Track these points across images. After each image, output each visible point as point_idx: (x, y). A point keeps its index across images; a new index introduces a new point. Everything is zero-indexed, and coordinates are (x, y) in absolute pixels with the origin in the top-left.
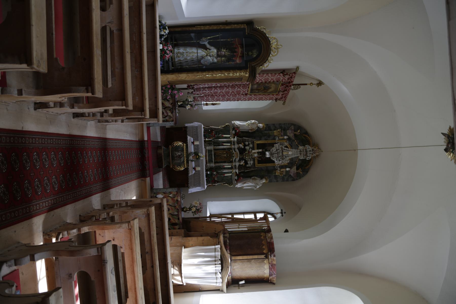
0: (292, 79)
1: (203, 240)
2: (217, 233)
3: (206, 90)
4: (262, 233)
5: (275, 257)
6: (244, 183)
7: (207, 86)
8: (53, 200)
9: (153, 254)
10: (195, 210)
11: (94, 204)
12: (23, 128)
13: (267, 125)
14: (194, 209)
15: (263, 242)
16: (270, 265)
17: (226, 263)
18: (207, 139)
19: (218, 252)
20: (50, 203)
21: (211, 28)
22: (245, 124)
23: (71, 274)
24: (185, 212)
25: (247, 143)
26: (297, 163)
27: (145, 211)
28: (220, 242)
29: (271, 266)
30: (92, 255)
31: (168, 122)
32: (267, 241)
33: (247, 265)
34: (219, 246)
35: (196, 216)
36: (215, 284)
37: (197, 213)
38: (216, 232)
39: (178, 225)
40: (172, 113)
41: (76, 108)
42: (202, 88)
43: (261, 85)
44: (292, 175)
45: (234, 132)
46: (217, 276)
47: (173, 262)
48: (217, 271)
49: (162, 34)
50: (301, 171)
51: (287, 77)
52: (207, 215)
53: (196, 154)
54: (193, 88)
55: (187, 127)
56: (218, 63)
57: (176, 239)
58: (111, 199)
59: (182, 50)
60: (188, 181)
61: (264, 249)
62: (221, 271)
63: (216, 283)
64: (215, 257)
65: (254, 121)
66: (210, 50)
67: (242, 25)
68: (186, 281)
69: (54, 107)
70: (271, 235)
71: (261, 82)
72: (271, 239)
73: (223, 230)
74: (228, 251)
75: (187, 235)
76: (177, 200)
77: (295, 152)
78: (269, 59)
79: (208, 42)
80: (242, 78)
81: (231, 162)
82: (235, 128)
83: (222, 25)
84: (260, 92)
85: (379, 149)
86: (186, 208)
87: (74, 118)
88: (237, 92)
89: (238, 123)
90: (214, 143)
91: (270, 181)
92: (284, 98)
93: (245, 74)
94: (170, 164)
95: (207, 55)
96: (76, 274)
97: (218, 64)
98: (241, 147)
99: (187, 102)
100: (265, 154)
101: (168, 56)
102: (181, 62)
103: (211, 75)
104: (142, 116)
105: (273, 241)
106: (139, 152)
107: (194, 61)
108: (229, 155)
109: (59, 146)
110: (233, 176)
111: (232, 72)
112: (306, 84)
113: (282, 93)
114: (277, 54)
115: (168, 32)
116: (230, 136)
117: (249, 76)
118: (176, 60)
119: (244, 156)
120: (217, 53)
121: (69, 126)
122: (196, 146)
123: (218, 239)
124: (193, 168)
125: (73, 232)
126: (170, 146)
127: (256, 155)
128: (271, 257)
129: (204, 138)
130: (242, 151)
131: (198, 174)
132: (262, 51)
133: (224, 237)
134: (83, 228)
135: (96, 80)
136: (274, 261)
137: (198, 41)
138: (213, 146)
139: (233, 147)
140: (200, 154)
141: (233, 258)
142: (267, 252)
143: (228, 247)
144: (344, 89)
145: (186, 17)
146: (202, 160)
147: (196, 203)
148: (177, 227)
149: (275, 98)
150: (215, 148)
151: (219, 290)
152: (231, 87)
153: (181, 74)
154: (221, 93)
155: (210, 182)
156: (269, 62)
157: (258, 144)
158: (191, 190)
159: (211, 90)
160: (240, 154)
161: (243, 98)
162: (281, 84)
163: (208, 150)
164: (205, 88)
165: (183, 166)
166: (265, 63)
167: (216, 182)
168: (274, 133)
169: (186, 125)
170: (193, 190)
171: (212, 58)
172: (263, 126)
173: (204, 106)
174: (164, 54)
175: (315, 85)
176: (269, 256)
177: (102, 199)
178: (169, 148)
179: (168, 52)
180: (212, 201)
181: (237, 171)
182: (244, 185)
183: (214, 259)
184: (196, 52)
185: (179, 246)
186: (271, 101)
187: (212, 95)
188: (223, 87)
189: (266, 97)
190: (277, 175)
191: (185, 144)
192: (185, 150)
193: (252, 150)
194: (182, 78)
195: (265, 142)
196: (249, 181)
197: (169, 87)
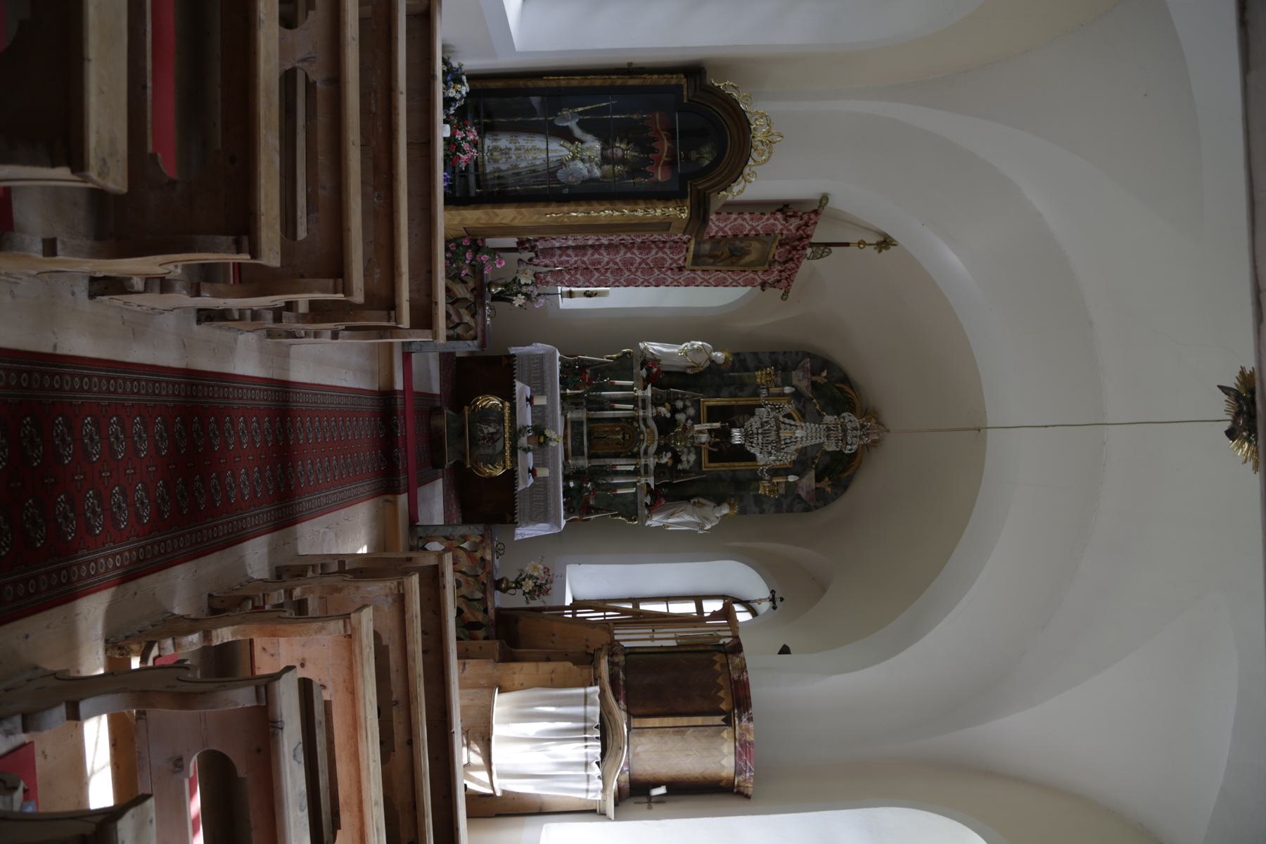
0: (808, 228)
3: (569, 256)
5: (751, 723)
6: (671, 515)
7: (574, 245)
8: (137, 549)
10: (531, 588)
11: (250, 565)
12: (55, 347)
13: (736, 355)
14: (528, 585)
15: (720, 681)
16: (737, 744)
17: (615, 737)
18: (568, 391)
19: (593, 704)
22: (676, 350)
23: (180, 759)
24: (504, 591)
25: (680, 404)
26: (816, 461)
27: (393, 586)
28: (600, 678)
29: (741, 746)
30: (240, 707)
31: (461, 342)
34: (597, 688)
35: (534, 604)
36: (583, 796)
37: (538, 596)
38: (588, 651)
39: (484, 629)
40: (473, 316)
43: (722, 243)
44: (803, 494)
45: (644, 373)
46: (588, 773)
47: (467, 732)
49: (451, 95)
50: (829, 486)
51: (795, 222)
54: (533, 249)
55: (514, 356)
56: (605, 180)
59: (504, 142)
60: (514, 507)
61: (722, 700)
62: (599, 759)
64: (585, 719)
65: (700, 343)
66: (582, 142)
67: (674, 76)
68: (502, 785)
69: (145, 291)
70: (741, 662)
71: (723, 236)
73: (610, 644)
76: (483, 559)
78: (746, 170)
79: (577, 120)
80: (671, 223)
81: (636, 455)
82: (649, 362)
84: (721, 264)
86: (507, 581)
87: (200, 324)
89: (655, 348)
91: (743, 511)
92: (784, 281)
95: (574, 158)
98: (663, 415)
99: (515, 288)
100: (729, 436)
102: (502, 174)
103: (583, 214)
104: (389, 321)
105: (747, 678)
107: (539, 171)
108: (630, 437)
111: (643, 206)
112: (847, 244)
113: (780, 268)
116: (632, 382)
117: (690, 219)
119: (670, 440)
120: (602, 154)
121: (184, 346)
122: (539, 409)
123: (596, 669)
124: (530, 471)
127: (704, 438)
128: (742, 721)
129: (561, 389)
130: (666, 426)
131: (542, 486)
133: (612, 664)
134: (219, 630)
136: (750, 735)
137: (551, 118)
138: (585, 409)
139: (641, 413)
140: (548, 433)
141: (636, 723)
142: (732, 706)
143: (622, 693)
144: (953, 259)
146: (555, 449)
147: (535, 568)
148: (481, 633)
149: (759, 281)
150: (590, 417)
151: (593, 811)
152: (639, 248)
153: (499, 208)
154: (611, 265)
156: (745, 181)
157: (710, 408)
158: (522, 532)
159: (584, 255)
160: (660, 435)
162: (777, 243)
163: (572, 422)
164: (568, 248)
166: (734, 182)
167: (593, 511)
168: (755, 377)
169: (513, 350)
170: (527, 532)
171: (588, 165)
172: (726, 358)
177: (273, 550)
178: (464, 415)
179: (464, 145)
180: (580, 564)
181: (651, 481)
182: (670, 520)
183: (581, 725)
184: (545, 147)
185: (484, 687)
186: (749, 288)
187: (587, 269)
189: (736, 278)
190: (761, 495)
191: (507, 404)
192: (507, 421)
193: (693, 425)
195: (731, 401)
196: (681, 509)
197: (466, 242)
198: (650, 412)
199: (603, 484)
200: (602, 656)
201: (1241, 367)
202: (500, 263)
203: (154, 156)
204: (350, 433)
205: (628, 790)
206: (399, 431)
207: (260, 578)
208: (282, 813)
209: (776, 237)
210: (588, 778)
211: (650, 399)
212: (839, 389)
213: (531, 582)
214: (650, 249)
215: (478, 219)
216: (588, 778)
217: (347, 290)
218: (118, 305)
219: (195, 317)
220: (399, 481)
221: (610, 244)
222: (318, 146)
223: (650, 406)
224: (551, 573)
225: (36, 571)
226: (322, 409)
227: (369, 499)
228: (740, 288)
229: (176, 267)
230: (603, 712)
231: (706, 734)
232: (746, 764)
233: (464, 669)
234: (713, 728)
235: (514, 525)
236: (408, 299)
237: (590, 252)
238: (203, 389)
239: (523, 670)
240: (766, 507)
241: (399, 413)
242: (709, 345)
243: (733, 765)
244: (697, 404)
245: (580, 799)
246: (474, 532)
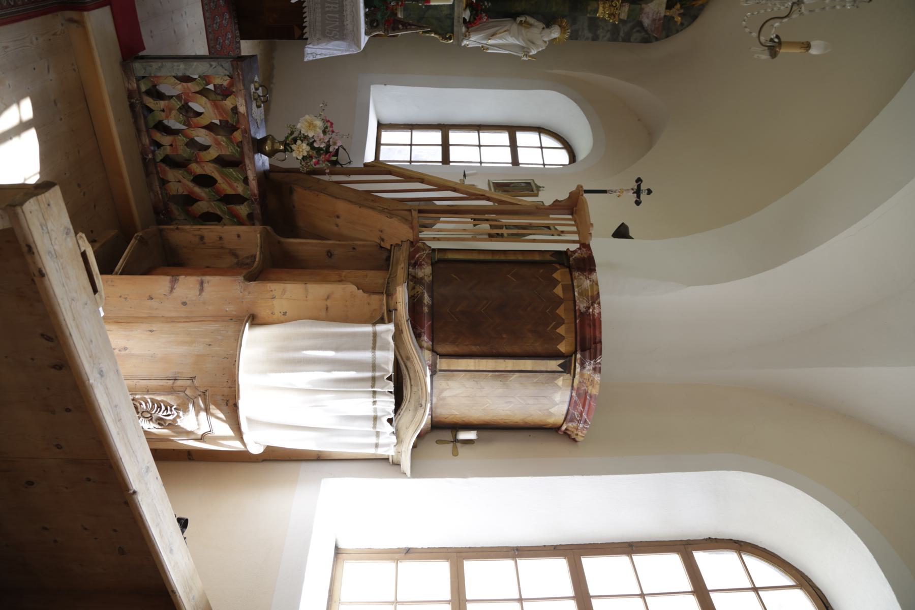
4: (557, 269)
6: (492, 36)
10: (305, 154)
15: (561, 311)
16: (574, 394)
17: (414, 389)
19: (385, 348)
28: (396, 310)
29: (578, 395)
32: (575, 305)
34: (391, 327)
38: (383, 244)
39: (246, 203)
44: (646, 22)
46: (377, 430)
48: (379, 414)
50: (680, 15)
60: (302, 20)
61: (561, 338)
62: (392, 416)
63: (377, 446)
70: (592, 286)
72: (592, 304)
74: (425, 338)
76: (235, 109)
86: (273, 140)
91: (574, 36)
105: (600, 314)
110: (456, 9)
128: (584, 368)
141: (443, 364)
142: (572, 349)
143: (427, 324)
147: (311, 125)
148: (243, 210)
155: (377, 25)
158: (313, 50)
167: (400, 26)
170: (319, 51)
180: (385, 85)
182: (491, 42)
183: (369, 374)
190: (598, 18)
196: (505, 29)
210: (378, 434)
216: (378, 434)
224: (335, 129)
230: (399, 357)
232: (581, 415)
233: (202, 290)
234: (545, 374)
240: (600, 32)
243: (565, 412)
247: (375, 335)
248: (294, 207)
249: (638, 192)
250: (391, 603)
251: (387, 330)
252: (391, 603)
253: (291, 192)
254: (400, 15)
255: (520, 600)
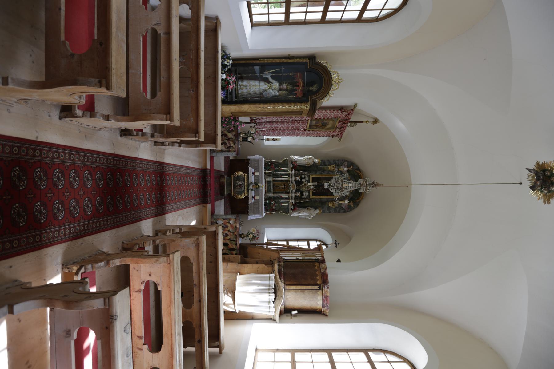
0: (349, 116)
1: (258, 268)
2: (272, 260)
3: (267, 125)
5: (328, 289)
7: (269, 121)
8: (84, 225)
9: (201, 287)
11: (143, 230)
12: (37, 137)
13: (322, 160)
14: (251, 236)
15: (317, 273)
16: (323, 297)
17: (280, 293)
18: (267, 171)
19: (272, 280)
20: (77, 230)
21: (274, 61)
22: (302, 159)
23: (69, 331)
24: (243, 238)
25: (303, 176)
27: (195, 240)
28: (275, 271)
29: (325, 297)
30: (96, 308)
31: (230, 153)
33: (300, 295)
34: (273, 275)
35: (252, 242)
36: (268, 313)
37: (254, 240)
38: (271, 260)
40: (234, 144)
41: (111, 120)
42: (264, 122)
43: (319, 121)
44: (344, 207)
45: (292, 166)
46: (270, 305)
47: (227, 289)
49: (226, 63)
50: (352, 204)
51: (345, 113)
52: (264, 242)
53: (256, 184)
54: (255, 122)
55: (249, 159)
56: (280, 96)
57: (232, 266)
58: (166, 225)
59: (245, 83)
60: (248, 209)
61: (318, 280)
62: (274, 301)
64: (269, 286)
65: (310, 156)
66: (272, 83)
67: (305, 59)
68: (238, 309)
69: (83, 117)
70: (325, 266)
71: (320, 119)
72: (325, 270)
73: (278, 258)
74: (282, 279)
75: (243, 262)
76: (236, 227)
77: (355, 184)
78: (330, 92)
79: (270, 75)
80: (303, 112)
81: (288, 193)
82: (293, 162)
83: (285, 59)
84: (319, 128)
85: (444, 184)
86: (244, 234)
87: (122, 137)
88: (296, 127)
89: (296, 158)
90: (273, 175)
91: (323, 212)
92: (340, 135)
93: (305, 107)
94: (232, 192)
95: (269, 89)
96: (78, 329)
97: (279, 97)
99: (249, 134)
100: (323, 186)
101: (231, 86)
102: (244, 94)
103: (272, 108)
104: (196, 138)
105: (327, 272)
106: (201, 179)
107: (257, 93)
109: (97, 165)
111: (293, 105)
112: (362, 122)
113: (339, 130)
114: (338, 87)
115: (232, 62)
116: (288, 169)
117: (310, 110)
118: (240, 92)
119: (300, 187)
120: (279, 87)
121: (114, 145)
122: (257, 177)
123: (273, 267)
124: (253, 197)
125: (99, 266)
126: (232, 176)
127: (312, 187)
129: (265, 170)
130: (299, 183)
131: (257, 202)
132: (324, 85)
133: (279, 265)
134: (114, 260)
135: (114, 72)
136: (328, 293)
137: (261, 75)
138: (272, 177)
139: (290, 179)
140: (259, 184)
141: (287, 287)
142: (321, 283)
143: (283, 276)
144: (401, 125)
145: (250, 48)
146: (262, 190)
147: (254, 230)
148: (234, 252)
149: (331, 135)
151: (271, 319)
152: (291, 123)
153: (243, 105)
154: (282, 128)
155: (268, 210)
156: (330, 96)
157: (313, 178)
159: (272, 125)
160: (297, 186)
161: (301, 134)
162: (338, 121)
164: (267, 122)
165: (243, 195)
166: (326, 96)
167: (274, 211)
168: (328, 168)
169: (249, 157)
170: (252, 217)
171: (274, 91)
172: (319, 161)
173: (266, 141)
174: (228, 84)
175: (371, 123)
176: (323, 287)
177: (154, 224)
178: (231, 178)
179: (231, 82)
180: (269, 228)
181: (293, 201)
182: (299, 214)
183: (268, 288)
184: (259, 84)
185: (234, 273)
186: (328, 137)
187: (273, 130)
188: (283, 122)
189: (324, 134)
191: (246, 174)
192: (246, 180)
193: (307, 183)
194: (244, 109)
197: (232, 118)
198: (294, 179)
199: (277, 202)
200: (276, 262)
201: (537, 161)
202: (243, 125)
203: (64, 43)
204: (189, 182)
205: (284, 311)
206: (208, 182)
207: (146, 235)
208: (114, 361)
209: (338, 119)
211: (293, 174)
212: (356, 172)
213: (252, 235)
214: (295, 123)
215: (236, 109)
217: (171, 120)
218: (75, 124)
219: (119, 134)
220: (207, 199)
221: (281, 121)
222: (161, 60)
223: (293, 176)
224: (259, 232)
225: (19, 237)
226: (178, 173)
227: (197, 205)
228: (325, 137)
229: (80, 97)
231: (312, 292)
233: (227, 266)
235: (247, 215)
236: (204, 130)
237: (274, 124)
238: (123, 162)
239: (248, 267)
240: (331, 211)
241: (208, 176)
242: (313, 157)
244: (309, 176)
245: (267, 314)
246: (232, 219)
247: (270, 277)
248: (247, 252)
249: (336, 244)
250: (273, 362)
251: (273, 275)
252: (273, 362)
253: (247, 248)
254: (274, 208)
255: (312, 362)
